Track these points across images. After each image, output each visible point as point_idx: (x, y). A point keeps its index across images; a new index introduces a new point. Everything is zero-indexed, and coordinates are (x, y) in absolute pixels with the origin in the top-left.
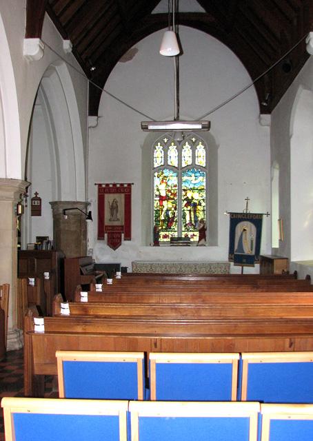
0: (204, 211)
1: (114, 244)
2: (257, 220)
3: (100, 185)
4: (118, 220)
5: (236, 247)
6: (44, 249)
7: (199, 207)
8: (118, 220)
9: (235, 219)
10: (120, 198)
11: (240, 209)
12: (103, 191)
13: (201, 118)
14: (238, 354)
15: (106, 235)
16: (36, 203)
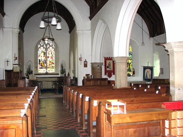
0: (132, 66)
1: (110, 76)
2: (152, 69)
3: (105, 57)
4: (111, 69)
5: (145, 77)
6: (90, 78)
7: (130, 64)
8: (111, 69)
9: (145, 68)
10: (111, 62)
11: (146, 65)
12: (106, 59)
13: (161, 43)
14: (93, 122)
15: (107, 73)
16: (86, 63)
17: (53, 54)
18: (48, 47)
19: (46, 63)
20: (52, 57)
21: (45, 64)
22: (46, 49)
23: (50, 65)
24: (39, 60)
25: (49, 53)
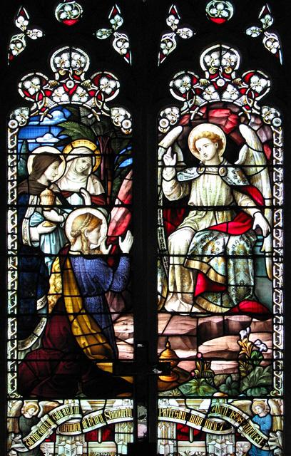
13: (224, 242)
17: (251, 150)
18: (168, 45)
19: (144, 306)
20: (244, 201)
21: (125, 328)
22: (146, 87)
23: (200, 335)
24: (30, 254)
25: (182, 141)
